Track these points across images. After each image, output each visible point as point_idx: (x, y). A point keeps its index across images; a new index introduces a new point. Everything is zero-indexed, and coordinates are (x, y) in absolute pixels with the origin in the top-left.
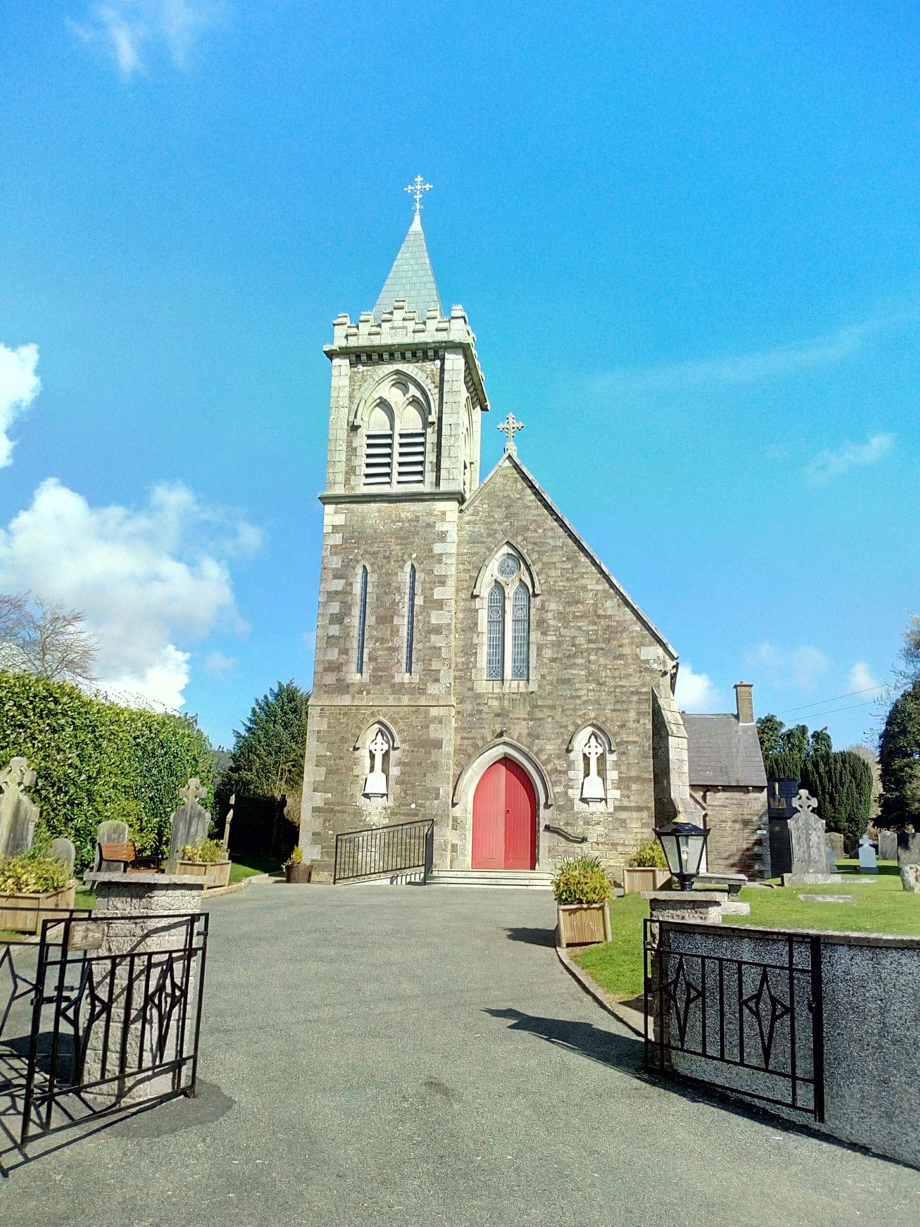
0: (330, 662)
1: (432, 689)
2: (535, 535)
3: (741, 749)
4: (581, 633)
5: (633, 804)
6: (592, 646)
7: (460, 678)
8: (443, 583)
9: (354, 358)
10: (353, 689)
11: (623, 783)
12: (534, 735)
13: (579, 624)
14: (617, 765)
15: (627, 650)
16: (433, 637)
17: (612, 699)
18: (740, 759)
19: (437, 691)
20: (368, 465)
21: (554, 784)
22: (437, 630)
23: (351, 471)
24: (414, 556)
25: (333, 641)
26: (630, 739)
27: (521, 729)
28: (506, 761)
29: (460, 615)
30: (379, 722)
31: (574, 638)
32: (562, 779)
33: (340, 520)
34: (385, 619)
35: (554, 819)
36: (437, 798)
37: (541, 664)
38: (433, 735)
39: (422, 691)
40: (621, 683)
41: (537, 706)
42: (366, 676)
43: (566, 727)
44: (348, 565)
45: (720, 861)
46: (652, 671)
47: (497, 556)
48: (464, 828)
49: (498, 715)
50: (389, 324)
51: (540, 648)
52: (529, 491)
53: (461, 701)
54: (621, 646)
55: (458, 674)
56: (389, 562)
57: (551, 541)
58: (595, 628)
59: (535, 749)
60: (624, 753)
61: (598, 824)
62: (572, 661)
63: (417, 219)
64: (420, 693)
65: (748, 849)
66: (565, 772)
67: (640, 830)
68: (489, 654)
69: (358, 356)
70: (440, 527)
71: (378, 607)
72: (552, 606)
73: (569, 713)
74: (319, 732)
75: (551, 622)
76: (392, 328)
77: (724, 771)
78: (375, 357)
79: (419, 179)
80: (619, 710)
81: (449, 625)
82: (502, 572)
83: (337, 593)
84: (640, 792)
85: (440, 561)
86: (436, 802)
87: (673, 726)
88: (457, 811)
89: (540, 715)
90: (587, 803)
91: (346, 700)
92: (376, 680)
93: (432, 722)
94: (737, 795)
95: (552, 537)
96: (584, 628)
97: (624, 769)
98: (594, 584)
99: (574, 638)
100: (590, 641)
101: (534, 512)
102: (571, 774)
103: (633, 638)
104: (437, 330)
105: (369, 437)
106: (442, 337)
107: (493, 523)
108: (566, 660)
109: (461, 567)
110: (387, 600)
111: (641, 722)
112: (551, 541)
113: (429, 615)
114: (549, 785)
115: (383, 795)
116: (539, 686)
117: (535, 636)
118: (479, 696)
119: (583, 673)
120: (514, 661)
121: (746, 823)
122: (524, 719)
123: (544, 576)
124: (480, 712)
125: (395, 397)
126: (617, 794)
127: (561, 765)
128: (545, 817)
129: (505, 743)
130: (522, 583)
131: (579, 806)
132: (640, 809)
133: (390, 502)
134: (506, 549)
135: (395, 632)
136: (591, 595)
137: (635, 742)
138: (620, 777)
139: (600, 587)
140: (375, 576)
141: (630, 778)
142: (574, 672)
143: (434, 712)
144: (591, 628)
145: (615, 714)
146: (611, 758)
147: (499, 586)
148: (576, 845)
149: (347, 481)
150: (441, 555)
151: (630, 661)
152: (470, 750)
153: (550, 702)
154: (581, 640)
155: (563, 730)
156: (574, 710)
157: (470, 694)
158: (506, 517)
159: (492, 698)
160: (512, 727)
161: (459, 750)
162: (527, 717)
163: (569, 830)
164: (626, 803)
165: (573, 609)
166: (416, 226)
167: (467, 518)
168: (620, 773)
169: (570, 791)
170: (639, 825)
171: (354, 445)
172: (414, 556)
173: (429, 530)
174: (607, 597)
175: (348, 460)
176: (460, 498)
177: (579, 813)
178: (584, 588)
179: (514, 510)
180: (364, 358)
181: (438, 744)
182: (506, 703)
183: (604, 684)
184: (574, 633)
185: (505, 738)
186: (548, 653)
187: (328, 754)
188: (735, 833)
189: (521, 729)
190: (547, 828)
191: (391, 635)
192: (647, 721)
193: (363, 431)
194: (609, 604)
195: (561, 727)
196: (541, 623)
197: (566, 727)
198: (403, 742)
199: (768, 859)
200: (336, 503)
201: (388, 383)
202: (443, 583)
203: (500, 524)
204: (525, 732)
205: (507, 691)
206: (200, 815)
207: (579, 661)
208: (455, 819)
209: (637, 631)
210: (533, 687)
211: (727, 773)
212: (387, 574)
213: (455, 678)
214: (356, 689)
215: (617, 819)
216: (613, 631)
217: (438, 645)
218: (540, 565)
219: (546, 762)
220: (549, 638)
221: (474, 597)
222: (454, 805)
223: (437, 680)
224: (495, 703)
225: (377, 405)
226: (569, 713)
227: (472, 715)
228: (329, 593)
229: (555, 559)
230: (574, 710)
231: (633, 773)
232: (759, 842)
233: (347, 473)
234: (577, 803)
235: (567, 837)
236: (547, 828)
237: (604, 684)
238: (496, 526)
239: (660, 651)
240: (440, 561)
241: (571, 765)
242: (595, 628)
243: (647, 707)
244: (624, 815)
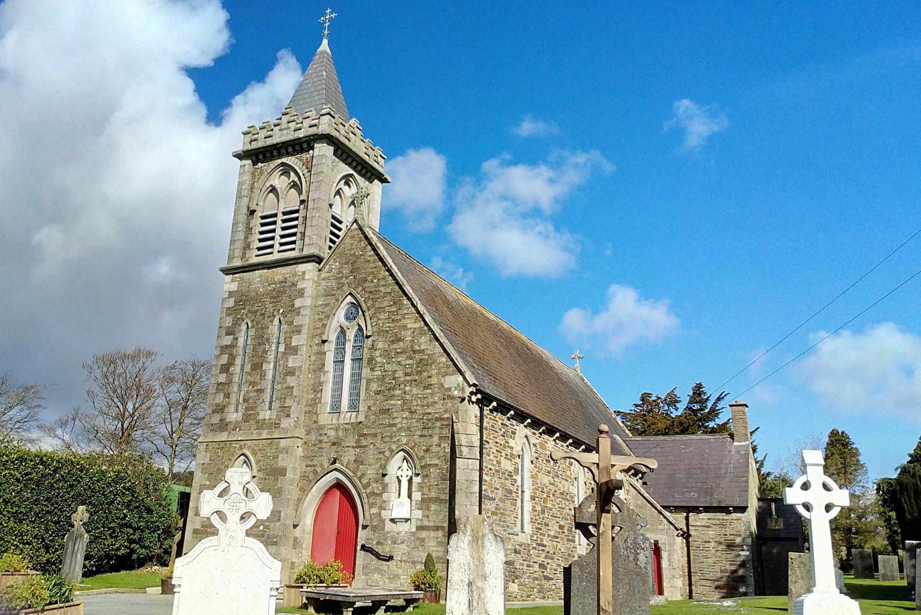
0: (217, 405)
1: (285, 423)
2: (372, 284)
3: (731, 469)
4: (399, 368)
5: (431, 524)
6: (408, 378)
7: (309, 412)
8: (299, 332)
9: (254, 158)
10: (231, 426)
11: (425, 503)
12: (358, 461)
13: (399, 360)
14: (421, 487)
15: (434, 380)
16: (289, 378)
17: (420, 426)
18: (727, 479)
19: (287, 426)
20: (261, 240)
21: (371, 506)
22: (291, 373)
23: (247, 246)
24: (281, 311)
25: (221, 387)
26: (432, 462)
27: (349, 456)
28: (339, 485)
29: (313, 358)
30: (243, 454)
33: (234, 287)
34: (257, 366)
35: (368, 539)
36: (279, 520)
37: (368, 397)
38: (281, 464)
39: (277, 425)
40: (428, 411)
42: (240, 414)
43: (383, 453)
44: (236, 323)
45: (704, 582)
46: (452, 398)
47: (342, 306)
48: (301, 547)
49: (334, 444)
50: (278, 127)
51: (369, 381)
52: (369, 247)
53: (308, 433)
54: (429, 377)
55: (308, 409)
56: (264, 318)
57: (382, 289)
58: (411, 362)
59: (359, 474)
60: (427, 476)
61: (403, 543)
62: (392, 393)
63: (325, 41)
64: (275, 428)
65: (734, 572)
66: (380, 495)
67: (435, 549)
68: (333, 390)
69: (257, 157)
70: (300, 285)
71: (253, 357)
72: (380, 345)
73: (386, 439)
74: (203, 464)
75: (378, 359)
76: (281, 130)
77: (708, 492)
78: (268, 155)
79: (329, 11)
80: (425, 436)
81: (300, 367)
82: (347, 318)
83: (227, 346)
84: (437, 512)
85: (298, 314)
86: (278, 524)
87: (463, 449)
88: (298, 532)
89: (364, 443)
90: (395, 523)
91: (223, 436)
92: (247, 418)
93: (281, 452)
94: (719, 515)
95: (383, 286)
96: (403, 363)
97: (426, 490)
98: (412, 324)
99: (395, 372)
100: (406, 374)
101: (372, 265)
102: (385, 496)
103: (440, 369)
104: (310, 127)
105: (263, 218)
106: (314, 130)
107: (342, 278)
108: (386, 392)
109: (317, 317)
110: (260, 350)
111: (442, 446)
112: (382, 289)
113: (287, 359)
114: (366, 506)
115: (407, 520)
116: (366, 417)
117: (366, 372)
118: (322, 427)
119: (399, 402)
120: (350, 395)
121: (731, 546)
122: (353, 447)
123: (375, 319)
124: (321, 441)
125: (280, 182)
126: (419, 514)
127: (376, 487)
128: (363, 536)
129: (336, 469)
130: (360, 329)
131: (389, 526)
132: (437, 528)
133: (269, 268)
134: (350, 299)
135: (263, 376)
136: (409, 333)
137: (437, 465)
139: (417, 325)
140: (254, 330)
141: (430, 499)
142: (392, 402)
143: (283, 443)
144: (408, 362)
145: (422, 439)
146: (417, 480)
147: (343, 332)
148: (384, 563)
149: (243, 257)
150: (299, 308)
151: (436, 390)
152: (311, 476)
153: (372, 431)
154: (400, 374)
155: (381, 456)
156: (391, 437)
157: (315, 426)
158: (351, 272)
160: (344, 454)
161: (304, 477)
162: (354, 445)
163: (378, 549)
164: (426, 523)
165: (395, 346)
166: (325, 46)
167: (324, 275)
169: (383, 512)
170: (435, 543)
171: (251, 225)
172: (281, 311)
173: (293, 288)
174: (422, 334)
175: (246, 238)
176: (318, 260)
177: (389, 532)
178: (405, 327)
179: (357, 265)
180: (261, 157)
181: (282, 472)
182: (340, 433)
183: (415, 412)
184: (394, 367)
185: (337, 465)
186: (374, 386)
188: (718, 554)
189: (349, 456)
190: (363, 547)
191: (261, 379)
192: (446, 445)
193: (259, 214)
194: (423, 339)
195: (380, 453)
196: (371, 360)
197: (383, 453)
198: (259, 471)
199: (751, 581)
200: (233, 274)
201: (277, 173)
202: (299, 332)
203: (346, 278)
204: (353, 458)
205: (342, 422)
206: (81, 536)
207: (397, 392)
208: (295, 539)
209: (444, 363)
210: (361, 418)
211: (711, 494)
212: (262, 328)
213: (305, 413)
214: (232, 426)
215: (418, 539)
216: (424, 364)
217: (292, 385)
218: (373, 310)
219: (366, 486)
220: (376, 373)
221: (324, 342)
222: (295, 526)
223: (288, 416)
224: (332, 433)
225: (270, 192)
226: (386, 439)
227: (315, 445)
228: (222, 347)
229: (385, 304)
230: (391, 437)
231: (433, 495)
232: (743, 565)
233: (244, 249)
234: (388, 522)
235: (377, 555)
236: (363, 547)
237: (415, 412)
238: (344, 281)
239: (461, 379)
240: (298, 314)
241: (385, 487)
242: (411, 362)
243: (446, 432)
244: (424, 534)
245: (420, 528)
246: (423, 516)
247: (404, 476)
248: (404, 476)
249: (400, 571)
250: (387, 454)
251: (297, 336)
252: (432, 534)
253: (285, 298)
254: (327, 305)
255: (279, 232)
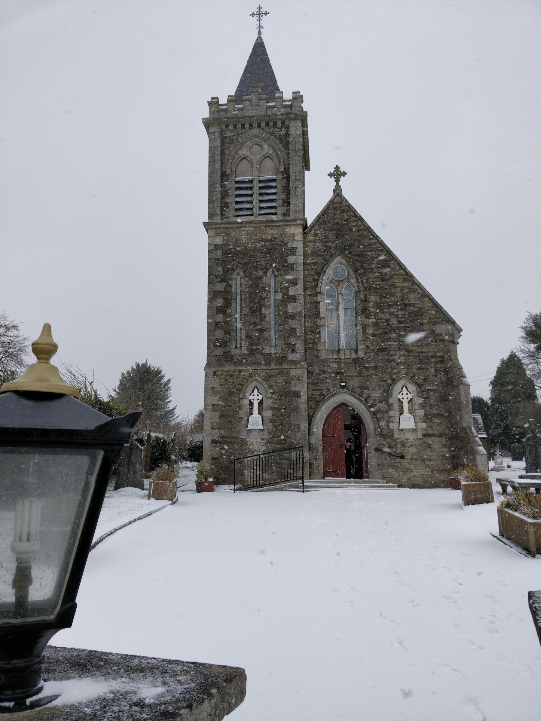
6: (401, 325)
11: (427, 418)
13: (392, 310)
14: (422, 406)
16: (290, 322)
24: (274, 265)
31: (388, 320)
32: (385, 416)
41: (364, 367)
66: (387, 412)
70: (290, 245)
83: (220, 292)
86: (298, 434)
95: (370, 251)
100: (399, 322)
107: (328, 242)
115: (414, 430)
119: (396, 343)
122: (356, 376)
132: (440, 436)
136: (399, 290)
137: (435, 390)
138: (425, 414)
142: (389, 343)
153: (373, 365)
154: (394, 321)
157: (317, 359)
159: (333, 362)
164: (430, 432)
168: (425, 411)
170: (440, 446)
172: (274, 265)
177: (397, 439)
178: (394, 285)
187: (220, 403)
220: (371, 320)
228: (215, 292)
242: (403, 312)
244: (430, 440)
245: (425, 436)
246: (428, 427)
247: (256, 400)
248: (256, 400)
249: (412, 467)
250: (389, 382)
251: (294, 288)
252: (437, 439)
253: (277, 255)
254: (315, 264)
255: (256, 198)
